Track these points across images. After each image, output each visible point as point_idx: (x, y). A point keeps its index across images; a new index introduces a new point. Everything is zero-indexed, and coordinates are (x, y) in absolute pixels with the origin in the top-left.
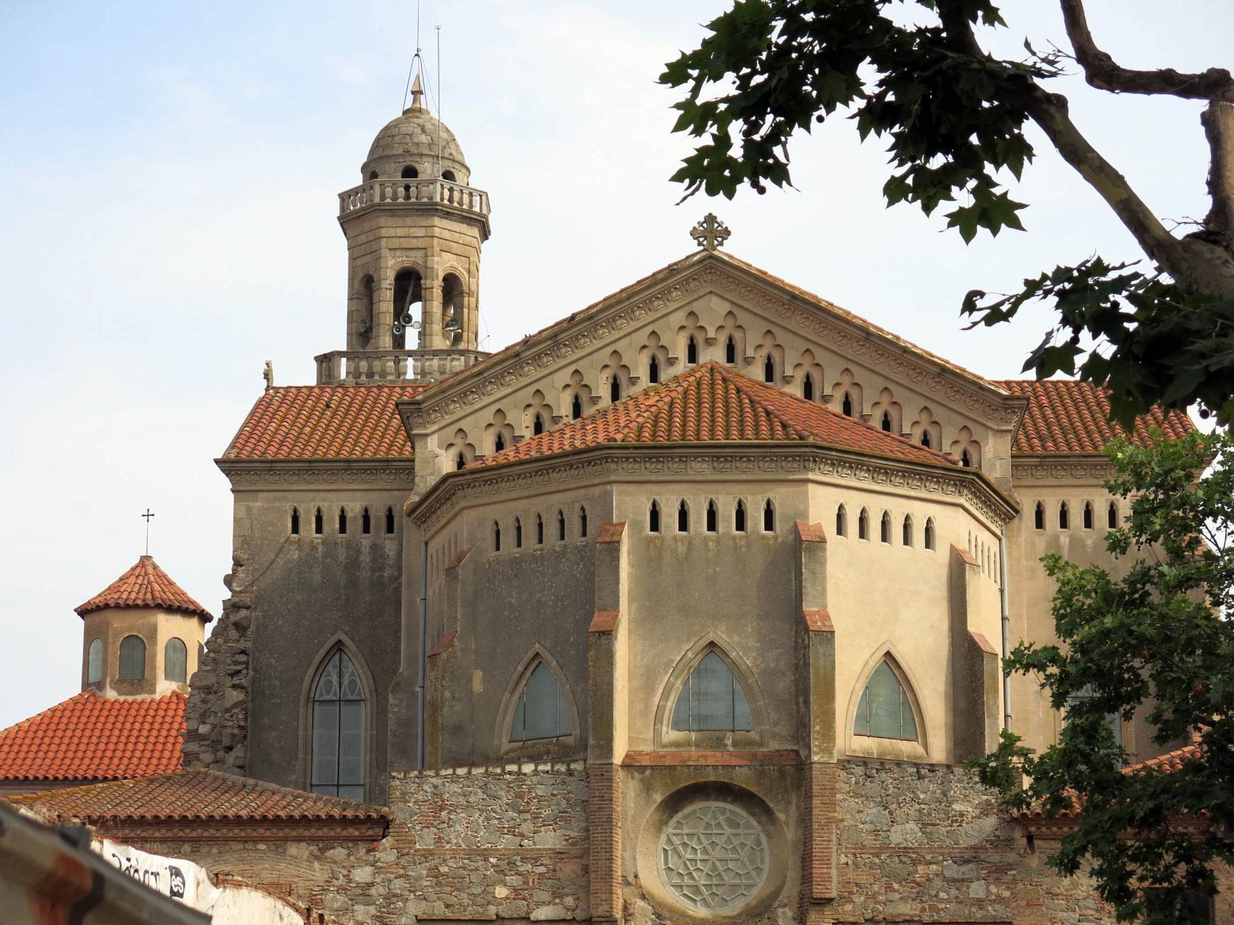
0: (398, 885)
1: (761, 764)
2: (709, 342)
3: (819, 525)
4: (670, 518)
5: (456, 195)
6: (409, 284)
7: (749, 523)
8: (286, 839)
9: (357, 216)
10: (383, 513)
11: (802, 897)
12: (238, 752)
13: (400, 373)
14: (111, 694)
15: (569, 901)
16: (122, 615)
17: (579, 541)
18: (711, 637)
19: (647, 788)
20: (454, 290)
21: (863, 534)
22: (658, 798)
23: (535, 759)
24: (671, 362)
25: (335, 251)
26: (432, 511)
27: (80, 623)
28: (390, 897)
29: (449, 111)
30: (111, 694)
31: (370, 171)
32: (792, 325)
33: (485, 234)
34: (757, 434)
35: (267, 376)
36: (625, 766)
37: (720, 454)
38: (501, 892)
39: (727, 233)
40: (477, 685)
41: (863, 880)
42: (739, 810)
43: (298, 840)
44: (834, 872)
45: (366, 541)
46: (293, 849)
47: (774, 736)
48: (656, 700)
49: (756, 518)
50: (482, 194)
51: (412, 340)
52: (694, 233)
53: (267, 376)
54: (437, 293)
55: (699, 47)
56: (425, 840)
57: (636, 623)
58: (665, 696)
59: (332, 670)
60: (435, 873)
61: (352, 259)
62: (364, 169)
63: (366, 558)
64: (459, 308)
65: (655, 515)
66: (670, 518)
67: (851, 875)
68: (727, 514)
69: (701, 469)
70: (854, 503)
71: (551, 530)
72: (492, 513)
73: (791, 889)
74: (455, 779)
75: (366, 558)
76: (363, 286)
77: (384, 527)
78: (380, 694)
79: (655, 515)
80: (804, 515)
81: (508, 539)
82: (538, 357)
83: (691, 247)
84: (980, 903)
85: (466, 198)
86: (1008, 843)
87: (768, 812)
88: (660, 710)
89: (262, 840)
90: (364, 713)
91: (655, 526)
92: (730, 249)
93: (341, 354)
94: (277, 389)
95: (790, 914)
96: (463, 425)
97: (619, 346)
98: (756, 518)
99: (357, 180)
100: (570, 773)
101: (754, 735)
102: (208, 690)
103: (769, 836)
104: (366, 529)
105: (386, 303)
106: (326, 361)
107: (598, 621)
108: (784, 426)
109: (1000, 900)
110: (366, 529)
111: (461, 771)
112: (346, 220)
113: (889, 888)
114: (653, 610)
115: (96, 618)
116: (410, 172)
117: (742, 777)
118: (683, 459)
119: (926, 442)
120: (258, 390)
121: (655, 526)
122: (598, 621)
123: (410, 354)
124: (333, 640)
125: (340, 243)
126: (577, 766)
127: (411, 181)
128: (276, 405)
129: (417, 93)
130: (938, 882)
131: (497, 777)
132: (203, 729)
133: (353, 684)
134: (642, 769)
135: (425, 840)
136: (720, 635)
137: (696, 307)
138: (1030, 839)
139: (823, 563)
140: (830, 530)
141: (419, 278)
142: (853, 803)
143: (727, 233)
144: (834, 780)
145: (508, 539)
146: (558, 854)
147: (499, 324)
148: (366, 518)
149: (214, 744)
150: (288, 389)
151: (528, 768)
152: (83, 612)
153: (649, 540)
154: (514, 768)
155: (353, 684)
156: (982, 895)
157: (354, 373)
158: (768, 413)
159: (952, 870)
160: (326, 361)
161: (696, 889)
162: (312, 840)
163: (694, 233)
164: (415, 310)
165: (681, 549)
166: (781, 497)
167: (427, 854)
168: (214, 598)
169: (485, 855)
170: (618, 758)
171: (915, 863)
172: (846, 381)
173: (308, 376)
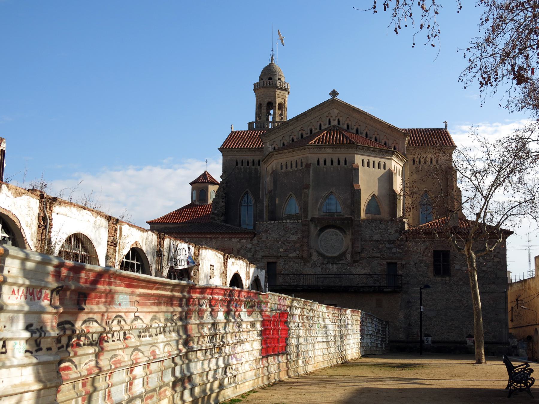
2: (334, 120)
3: (357, 164)
5: (281, 84)
7: (341, 163)
8: (232, 238)
10: (257, 161)
13: (268, 126)
16: (201, 183)
17: (301, 168)
18: (332, 190)
19: (316, 226)
20: (281, 107)
22: (319, 228)
23: (290, 219)
24: (325, 124)
27: (190, 186)
28: (255, 251)
31: (261, 78)
34: (343, 142)
36: (311, 220)
38: (281, 250)
39: (338, 94)
40: (277, 202)
42: (338, 231)
43: (234, 238)
44: (360, 246)
45: (253, 167)
46: (233, 240)
51: (271, 119)
52: (330, 94)
54: (277, 107)
56: (264, 238)
59: (245, 197)
60: (266, 245)
61: (257, 100)
62: (259, 78)
63: (253, 172)
64: (282, 111)
65: (318, 162)
70: (366, 158)
71: (294, 165)
73: (350, 250)
74: (271, 224)
75: (253, 172)
76: (259, 107)
77: (246, 164)
78: (256, 203)
79: (318, 162)
81: (284, 167)
82: (293, 124)
83: (330, 97)
84: (394, 253)
85: (284, 85)
87: (345, 232)
89: (226, 238)
90: (253, 208)
92: (339, 97)
93: (254, 122)
94: (234, 131)
95: (349, 256)
97: (312, 121)
99: (258, 80)
100: (298, 222)
102: (217, 203)
103: (345, 237)
104: (253, 165)
106: (250, 124)
108: (350, 141)
109: (399, 253)
110: (253, 165)
113: (373, 249)
119: (385, 144)
120: (230, 132)
123: (270, 122)
124: (246, 191)
126: (300, 221)
127: (271, 81)
128: (234, 135)
129: (272, 59)
130: (385, 249)
131: (281, 223)
132: (216, 212)
135: (264, 238)
137: (331, 111)
143: (338, 94)
145: (284, 167)
146: (295, 242)
147: (291, 114)
148: (253, 162)
150: (236, 132)
151: (288, 221)
152: (191, 184)
154: (285, 221)
156: (395, 251)
157: (257, 127)
158: (346, 137)
159: (388, 246)
160: (250, 124)
161: (327, 250)
162: (238, 238)
163: (330, 94)
164: (272, 112)
168: (219, 180)
173: (246, 128)
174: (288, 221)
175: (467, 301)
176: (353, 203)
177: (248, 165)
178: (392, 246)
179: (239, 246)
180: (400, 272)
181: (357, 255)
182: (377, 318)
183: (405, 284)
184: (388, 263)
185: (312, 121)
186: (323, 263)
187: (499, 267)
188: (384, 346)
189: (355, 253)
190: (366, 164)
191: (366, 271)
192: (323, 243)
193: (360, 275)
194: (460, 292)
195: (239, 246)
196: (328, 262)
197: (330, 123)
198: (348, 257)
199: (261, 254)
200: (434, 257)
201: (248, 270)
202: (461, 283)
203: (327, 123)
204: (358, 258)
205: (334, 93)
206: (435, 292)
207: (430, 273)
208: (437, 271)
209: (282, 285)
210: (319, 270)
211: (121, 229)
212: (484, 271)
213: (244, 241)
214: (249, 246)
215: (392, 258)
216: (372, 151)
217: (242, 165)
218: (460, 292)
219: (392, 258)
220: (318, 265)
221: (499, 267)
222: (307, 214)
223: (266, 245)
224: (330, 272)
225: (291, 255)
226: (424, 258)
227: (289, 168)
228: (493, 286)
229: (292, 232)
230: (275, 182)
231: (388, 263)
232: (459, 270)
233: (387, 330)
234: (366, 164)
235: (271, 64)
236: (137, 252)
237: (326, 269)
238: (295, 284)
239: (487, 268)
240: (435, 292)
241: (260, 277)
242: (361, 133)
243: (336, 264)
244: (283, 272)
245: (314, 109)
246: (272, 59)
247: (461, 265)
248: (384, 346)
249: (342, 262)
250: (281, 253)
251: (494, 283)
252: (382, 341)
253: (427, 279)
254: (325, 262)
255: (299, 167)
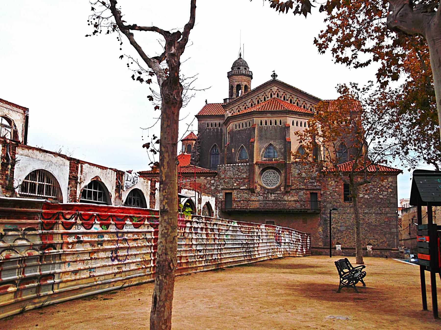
0: (218, 183)
1: (278, 164)
2: (274, 94)
4: (264, 123)
6: (239, 87)
7: (263, 123)
9: (230, 75)
11: (285, 185)
12: (199, 162)
14: (186, 154)
15: (246, 186)
19: (259, 168)
21: (297, 125)
22: (261, 169)
24: (268, 97)
25: (226, 82)
26: (227, 123)
28: (217, 185)
29: (245, 58)
30: (186, 154)
31: (232, 68)
32: (288, 91)
33: (252, 78)
35: (206, 102)
36: (256, 164)
37: (273, 113)
38: (235, 184)
39: (277, 76)
40: (233, 151)
41: (296, 182)
43: (202, 176)
46: (201, 178)
47: (281, 159)
48: (261, 153)
49: (278, 123)
50: (251, 72)
53: (206, 102)
55: (132, 25)
57: (258, 140)
58: (263, 153)
66: (264, 123)
67: (293, 182)
68: (273, 122)
69: (269, 115)
71: (244, 125)
72: (235, 123)
73: (283, 184)
74: (228, 166)
76: (231, 88)
80: (286, 122)
81: (238, 127)
82: (245, 97)
83: (271, 78)
84: (315, 186)
86: (321, 176)
87: (280, 171)
88: (262, 155)
91: (261, 124)
92: (277, 78)
96: (233, 109)
98: (278, 123)
100: (247, 165)
101: (278, 159)
105: (235, 90)
106: (225, 100)
107: (251, 140)
109: (319, 185)
110: (219, 126)
111: (229, 165)
112: (228, 77)
113: (300, 184)
114: (261, 137)
115: (184, 142)
116: (239, 68)
117: (275, 166)
118: (266, 113)
121: (261, 124)
122: (251, 140)
125: (228, 80)
126: (248, 164)
127: (239, 70)
129: (240, 55)
133: (217, 151)
134: (259, 164)
136: (272, 142)
137: (272, 88)
138: (324, 176)
139: (289, 130)
140: (291, 125)
141: (240, 86)
142: (294, 170)
143: (277, 76)
144: (291, 166)
145: (238, 127)
149: (195, 161)
153: (260, 127)
155: (217, 151)
159: (311, 181)
160: (225, 100)
161: (268, 184)
162: (204, 176)
165: (266, 128)
166: (282, 119)
167: (223, 178)
169: (233, 178)
170: (254, 163)
171: (304, 179)
172: (297, 100)
174: (240, 164)
175: (368, 220)
176: (285, 151)
177: (216, 126)
178: (314, 181)
179: (205, 181)
180: (320, 199)
181: (287, 188)
182: (296, 232)
183: (323, 207)
184: (310, 193)
185: (259, 95)
186: (264, 193)
187: (391, 195)
188: (304, 250)
189: (286, 186)
190: (295, 124)
191: (295, 198)
192: (264, 180)
193: (291, 201)
194: (363, 213)
195: (205, 181)
196: (268, 193)
197: (271, 97)
198: (282, 189)
199: (221, 187)
200: (344, 188)
201: (200, 197)
202: (364, 207)
203: (270, 96)
204: (289, 190)
205: (274, 75)
206: (344, 213)
207: (342, 201)
208: (346, 199)
209: (235, 208)
210: (261, 198)
211: (82, 167)
212: (381, 198)
213: (209, 178)
214: (213, 182)
215: (313, 190)
216: (300, 114)
217: (212, 126)
218: (363, 213)
219: (313, 190)
220: (261, 194)
221: (391, 195)
222: (253, 159)
223: (224, 181)
224: (269, 200)
225: (242, 188)
226: (337, 189)
227: (245, 127)
228: (387, 209)
229: (242, 172)
230: (231, 138)
231: (310, 193)
232: (362, 197)
233: (308, 239)
234: (295, 124)
235: (240, 58)
236: (99, 184)
237: (266, 198)
238: (245, 208)
239: (383, 196)
240: (344, 213)
241: (211, 203)
242: (294, 103)
243: (274, 194)
244: (236, 200)
245: (261, 86)
246: (240, 55)
247: (364, 194)
248: (304, 250)
249: (278, 192)
250: (235, 186)
251: (388, 207)
252: (302, 247)
253: (338, 204)
254: (266, 192)
255: (245, 127)
